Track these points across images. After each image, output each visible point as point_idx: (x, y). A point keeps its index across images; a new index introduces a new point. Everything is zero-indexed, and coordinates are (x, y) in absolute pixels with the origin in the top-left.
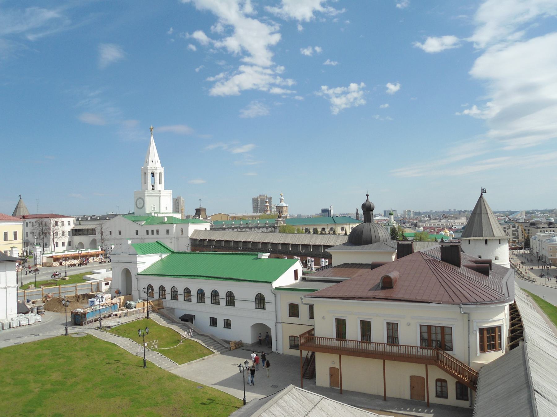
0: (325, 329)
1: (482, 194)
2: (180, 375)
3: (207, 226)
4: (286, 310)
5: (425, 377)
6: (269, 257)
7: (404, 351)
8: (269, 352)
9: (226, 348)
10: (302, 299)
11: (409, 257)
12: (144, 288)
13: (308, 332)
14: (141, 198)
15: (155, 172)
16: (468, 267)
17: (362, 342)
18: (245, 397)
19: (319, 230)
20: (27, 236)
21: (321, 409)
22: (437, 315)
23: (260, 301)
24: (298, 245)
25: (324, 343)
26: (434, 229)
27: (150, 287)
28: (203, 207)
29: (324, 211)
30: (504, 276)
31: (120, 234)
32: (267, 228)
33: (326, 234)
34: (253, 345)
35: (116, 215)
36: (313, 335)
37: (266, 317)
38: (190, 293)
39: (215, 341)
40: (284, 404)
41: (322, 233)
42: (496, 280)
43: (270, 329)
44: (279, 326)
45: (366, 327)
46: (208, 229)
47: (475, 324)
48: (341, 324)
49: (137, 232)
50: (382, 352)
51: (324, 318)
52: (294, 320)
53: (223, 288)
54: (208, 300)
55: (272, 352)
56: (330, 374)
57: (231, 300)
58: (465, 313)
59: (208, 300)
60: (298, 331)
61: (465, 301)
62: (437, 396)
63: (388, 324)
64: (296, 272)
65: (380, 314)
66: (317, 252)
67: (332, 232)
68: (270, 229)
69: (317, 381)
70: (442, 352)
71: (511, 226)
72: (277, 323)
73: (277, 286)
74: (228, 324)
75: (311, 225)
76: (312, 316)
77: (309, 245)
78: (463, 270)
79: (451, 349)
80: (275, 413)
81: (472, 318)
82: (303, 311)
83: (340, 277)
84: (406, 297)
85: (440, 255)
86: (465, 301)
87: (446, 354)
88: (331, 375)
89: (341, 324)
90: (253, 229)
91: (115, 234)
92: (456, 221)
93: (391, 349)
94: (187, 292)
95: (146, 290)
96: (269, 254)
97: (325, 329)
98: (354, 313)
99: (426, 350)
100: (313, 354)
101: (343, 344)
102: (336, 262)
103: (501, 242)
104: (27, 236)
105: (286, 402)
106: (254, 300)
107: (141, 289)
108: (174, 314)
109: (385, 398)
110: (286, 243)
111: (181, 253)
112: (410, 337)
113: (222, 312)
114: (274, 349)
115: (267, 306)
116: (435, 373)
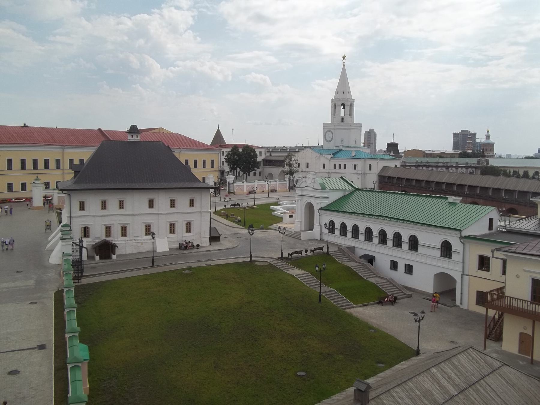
2: (359, 316)
4: (475, 262)
5: (531, 334)
6: (461, 202)
9: (405, 294)
12: (326, 224)
13: (498, 290)
15: (346, 103)
18: (418, 347)
20: (223, 164)
21: (501, 376)
24: (501, 189)
25: (514, 303)
27: (332, 223)
28: (395, 142)
31: (308, 167)
35: (306, 147)
36: (504, 293)
37: (452, 267)
38: (346, 228)
39: (394, 286)
41: (533, 178)
43: (453, 281)
44: (466, 278)
46: (399, 166)
50: (532, 311)
51: (518, 276)
54: (390, 243)
55: (455, 306)
57: (414, 244)
59: (390, 243)
64: (491, 221)
72: (463, 275)
73: (467, 235)
74: (409, 269)
76: (504, 273)
77: (515, 191)
80: (445, 370)
82: (495, 265)
94: (356, 229)
95: (328, 226)
96: (461, 198)
100: (501, 316)
104: (223, 164)
105: (459, 360)
106: (440, 247)
107: (323, 225)
111: (368, 191)
113: (403, 256)
114: (458, 302)
115: (453, 255)
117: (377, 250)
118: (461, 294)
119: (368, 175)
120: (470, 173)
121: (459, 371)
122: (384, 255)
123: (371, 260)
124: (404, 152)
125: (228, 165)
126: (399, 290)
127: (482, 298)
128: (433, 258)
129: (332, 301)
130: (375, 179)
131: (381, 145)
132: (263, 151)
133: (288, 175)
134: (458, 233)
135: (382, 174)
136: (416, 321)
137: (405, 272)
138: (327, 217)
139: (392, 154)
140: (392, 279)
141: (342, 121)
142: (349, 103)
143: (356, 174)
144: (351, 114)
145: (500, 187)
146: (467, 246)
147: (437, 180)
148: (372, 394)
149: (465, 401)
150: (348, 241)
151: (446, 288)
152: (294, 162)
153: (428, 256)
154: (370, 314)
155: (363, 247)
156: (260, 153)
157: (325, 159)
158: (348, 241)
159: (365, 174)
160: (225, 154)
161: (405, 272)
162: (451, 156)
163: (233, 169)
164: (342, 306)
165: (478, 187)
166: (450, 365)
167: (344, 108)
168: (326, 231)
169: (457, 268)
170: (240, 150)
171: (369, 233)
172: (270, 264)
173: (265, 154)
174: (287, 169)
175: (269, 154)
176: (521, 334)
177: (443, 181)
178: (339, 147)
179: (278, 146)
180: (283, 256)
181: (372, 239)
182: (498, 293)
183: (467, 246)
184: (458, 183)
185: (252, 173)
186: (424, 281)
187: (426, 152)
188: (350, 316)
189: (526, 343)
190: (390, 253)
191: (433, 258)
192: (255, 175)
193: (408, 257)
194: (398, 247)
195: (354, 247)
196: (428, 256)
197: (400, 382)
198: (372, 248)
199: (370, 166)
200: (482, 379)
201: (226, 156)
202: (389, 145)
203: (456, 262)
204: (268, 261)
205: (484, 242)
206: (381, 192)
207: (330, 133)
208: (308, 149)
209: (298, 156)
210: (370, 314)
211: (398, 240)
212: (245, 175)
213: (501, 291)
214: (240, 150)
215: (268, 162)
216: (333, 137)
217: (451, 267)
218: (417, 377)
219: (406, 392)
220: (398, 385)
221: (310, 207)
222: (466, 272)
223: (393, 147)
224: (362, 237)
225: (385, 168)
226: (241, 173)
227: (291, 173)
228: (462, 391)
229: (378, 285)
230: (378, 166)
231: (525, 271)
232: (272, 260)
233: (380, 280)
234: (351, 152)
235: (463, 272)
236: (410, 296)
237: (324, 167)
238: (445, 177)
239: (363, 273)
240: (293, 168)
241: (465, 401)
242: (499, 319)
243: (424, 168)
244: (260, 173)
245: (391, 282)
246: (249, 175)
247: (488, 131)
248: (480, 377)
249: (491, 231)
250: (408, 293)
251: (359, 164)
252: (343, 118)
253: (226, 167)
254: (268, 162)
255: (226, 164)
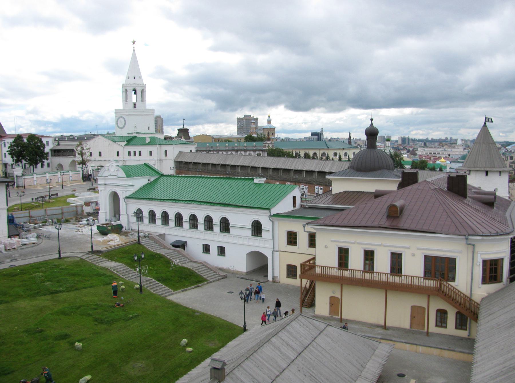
0: (326, 258)
1: (485, 123)
2: (176, 301)
3: (193, 148)
4: (284, 238)
6: (266, 182)
7: (407, 281)
8: (265, 281)
9: (220, 276)
10: (304, 227)
11: (415, 186)
13: (309, 261)
14: (122, 117)
16: (474, 198)
17: (365, 271)
18: (245, 323)
19: (319, 155)
20: (5, 156)
21: (326, 335)
22: (441, 247)
23: (257, 229)
25: (325, 272)
26: (430, 158)
29: (313, 134)
30: (507, 208)
31: (100, 155)
32: (255, 151)
33: (317, 159)
34: (248, 273)
36: (314, 263)
37: (262, 245)
39: (209, 268)
40: (291, 330)
41: (313, 158)
42: (500, 212)
44: (275, 253)
45: (369, 256)
46: (194, 151)
47: (479, 255)
48: (343, 254)
49: (118, 153)
51: (326, 247)
52: (292, 248)
53: (217, 215)
54: (201, 227)
55: (268, 281)
56: (330, 303)
57: (225, 225)
58: (470, 244)
59: (201, 227)
60: (297, 261)
61: (471, 232)
62: (437, 326)
63: (392, 254)
64: (294, 198)
65: (384, 244)
66: (322, 178)
67: (324, 158)
68: (257, 152)
69: (316, 310)
70: (445, 283)
71: (509, 158)
72: (273, 251)
73: (275, 213)
74: (222, 251)
75: (303, 149)
78: (468, 200)
79: (453, 279)
80: (283, 338)
81: (476, 250)
82: (303, 239)
83: (341, 204)
84: (412, 227)
85: (446, 185)
86: (471, 232)
87: (449, 284)
88: (331, 305)
89: (343, 254)
90: (239, 152)
91: (95, 156)
92: (453, 150)
93: (395, 279)
97: (326, 258)
98: (357, 243)
99: (430, 281)
101: (346, 274)
102: (337, 188)
103: (489, 174)
104: (5, 156)
106: (250, 227)
108: (164, 240)
109: (385, 327)
110: (278, 167)
112: (413, 268)
113: (215, 238)
115: (264, 234)
116: (436, 304)
117: (188, 235)
118: (273, 269)
119: (164, 161)
120: (258, 155)
121: (295, 337)
122: (195, 239)
123: (181, 245)
124: (194, 137)
125: (12, 157)
126: (215, 272)
127: (291, 271)
128: (245, 237)
129: (148, 289)
130: (172, 164)
131: (172, 131)
132: (51, 140)
133: (81, 165)
134: (267, 212)
135: (179, 160)
136: (242, 299)
137: (218, 255)
138: (134, 206)
139: (183, 139)
140: (205, 262)
141: (135, 107)
142: (141, 88)
143: (152, 160)
144: (143, 99)
145: (289, 168)
146: (276, 223)
147: (232, 164)
148: (227, 370)
149: (303, 362)
150: (158, 228)
151: (259, 264)
152: (86, 151)
153: (240, 237)
154: (187, 298)
155: (173, 233)
156: (48, 142)
157: (117, 147)
158: (158, 228)
159: (161, 160)
160: (8, 145)
161: (218, 255)
162: (239, 140)
163: (18, 161)
164: (162, 294)
165: (270, 168)
166: (286, 333)
167: (135, 93)
168: (134, 219)
169: (267, 246)
170: (25, 140)
171: (165, 217)
172: (82, 259)
173: (53, 144)
174: (78, 158)
175: (57, 144)
176: (331, 298)
177: (238, 164)
178: (132, 133)
179: (65, 134)
180: (94, 250)
181: (168, 223)
182: (310, 263)
183: (276, 223)
184: (252, 165)
185: (39, 165)
186: (237, 261)
187: (214, 137)
188: (169, 301)
189: (335, 304)
190: (202, 237)
191: (245, 237)
192: (42, 166)
193: (220, 239)
194: (209, 230)
195: (164, 234)
196: (240, 237)
197: (248, 356)
198: (184, 233)
199: (166, 152)
200: (313, 340)
201: (9, 147)
202: (180, 130)
203: (267, 240)
204: (79, 256)
205: (291, 219)
206: (179, 176)
207: (122, 119)
208: (100, 137)
209: (87, 145)
210: (187, 298)
211: (209, 223)
212: (32, 167)
213: (311, 262)
214: (25, 140)
215: (56, 152)
216: (125, 123)
217: (262, 245)
218: (261, 348)
219: (254, 363)
220: (247, 359)
221: (115, 196)
222: (277, 249)
223: (184, 132)
224: (172, 223)
225: (180, 153)
226: (28, 166)
227: (83, 163)
228: (300, 354)
229: (194, 269)
230: (174, 151)
231: (332, 241)
232: (82, 254)
233: (194, 265)
234: (145, 138)
235: (274, 248)
236: (225, 277)
237: (118, 155)
238: (232, 159)
239: (177, 261)
240: (85, 157)
241: (303, 362)
242: (310, 288)
243: (224, 153)
244: (48, 164)
245: (204, 265)
246: (36, 167)
247: (269, 116)
248: (312, 339)
249: (295, 208)
250: (223, 274)
251: (154, 149)
252: (135, 104)
253: (9, 160)
254: (56, 152)
255: (9, 157)
